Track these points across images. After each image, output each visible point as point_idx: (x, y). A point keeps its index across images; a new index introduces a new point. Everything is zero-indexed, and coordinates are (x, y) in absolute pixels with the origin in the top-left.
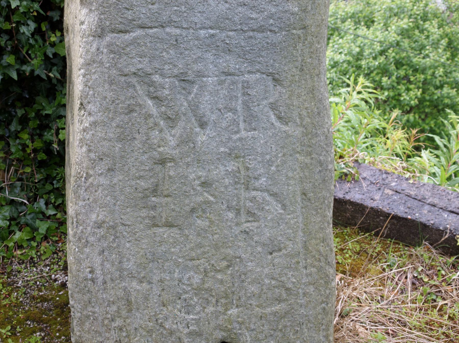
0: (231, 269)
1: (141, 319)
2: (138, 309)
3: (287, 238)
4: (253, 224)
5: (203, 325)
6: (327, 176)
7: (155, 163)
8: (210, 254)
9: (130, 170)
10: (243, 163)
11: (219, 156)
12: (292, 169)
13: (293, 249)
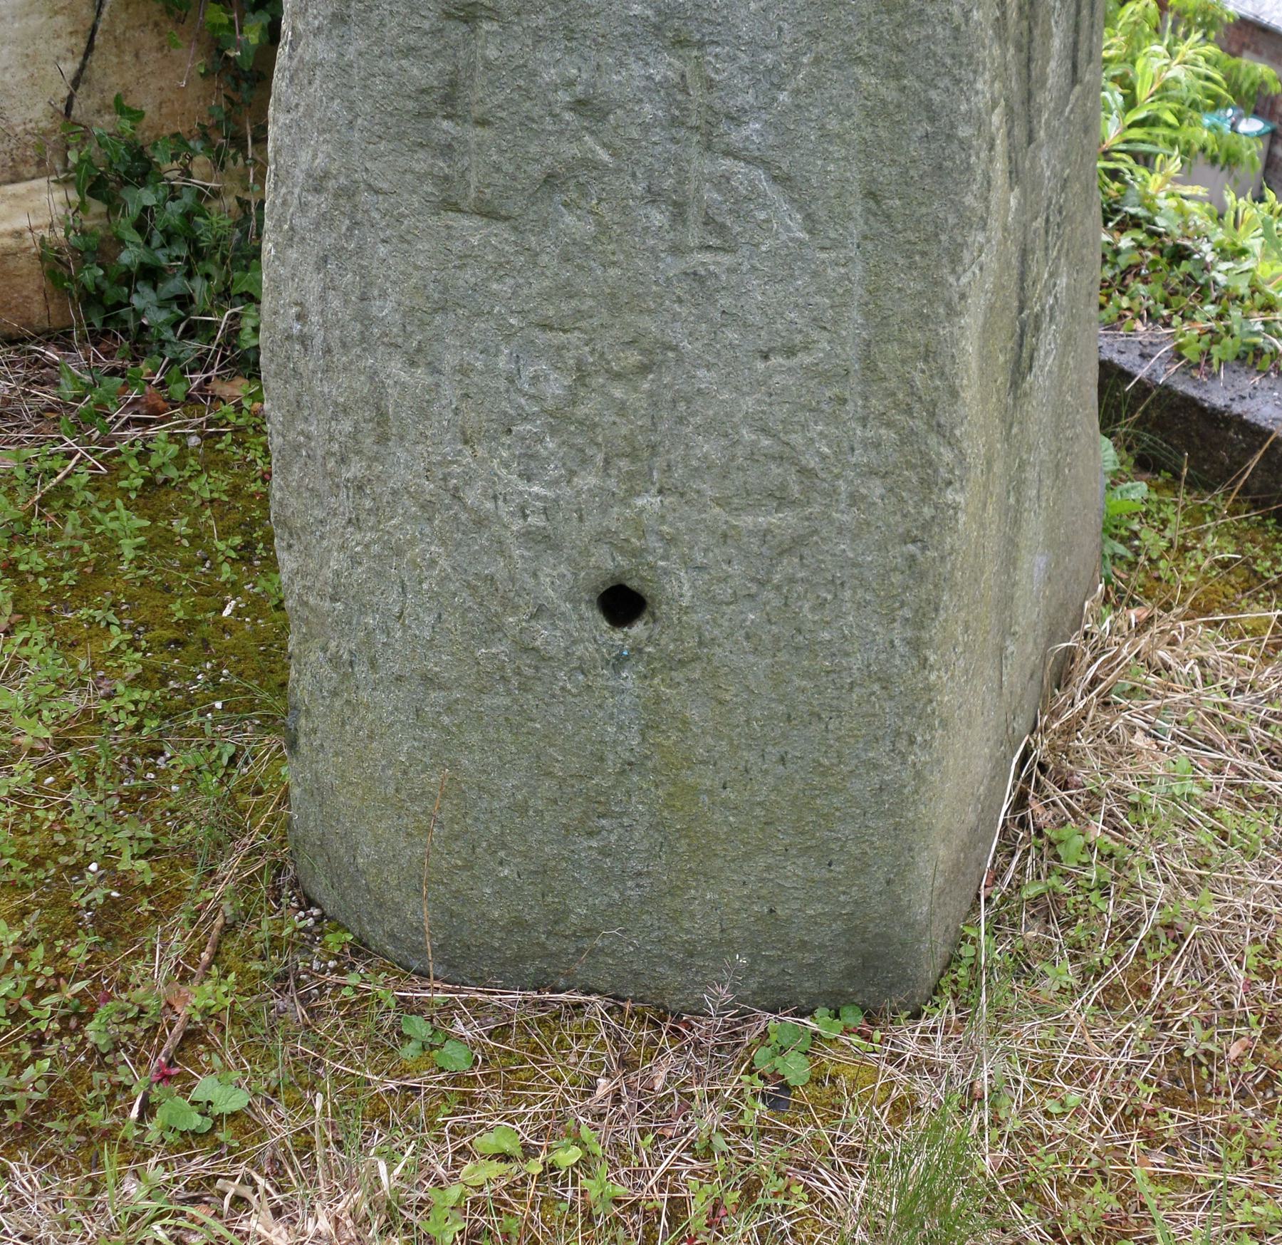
0: (651, 376)
1: (407, 467)
2: (402, 438)
3: (814, 320)
4: (719, 259)
5: (567, 520)
6: (953, 159)
7: (449, 16)
8: (596, 322)
9: (384, 26)
10: (698, 65)
11: (629, 29)
12: (837, 109)
13: (828, 355)
